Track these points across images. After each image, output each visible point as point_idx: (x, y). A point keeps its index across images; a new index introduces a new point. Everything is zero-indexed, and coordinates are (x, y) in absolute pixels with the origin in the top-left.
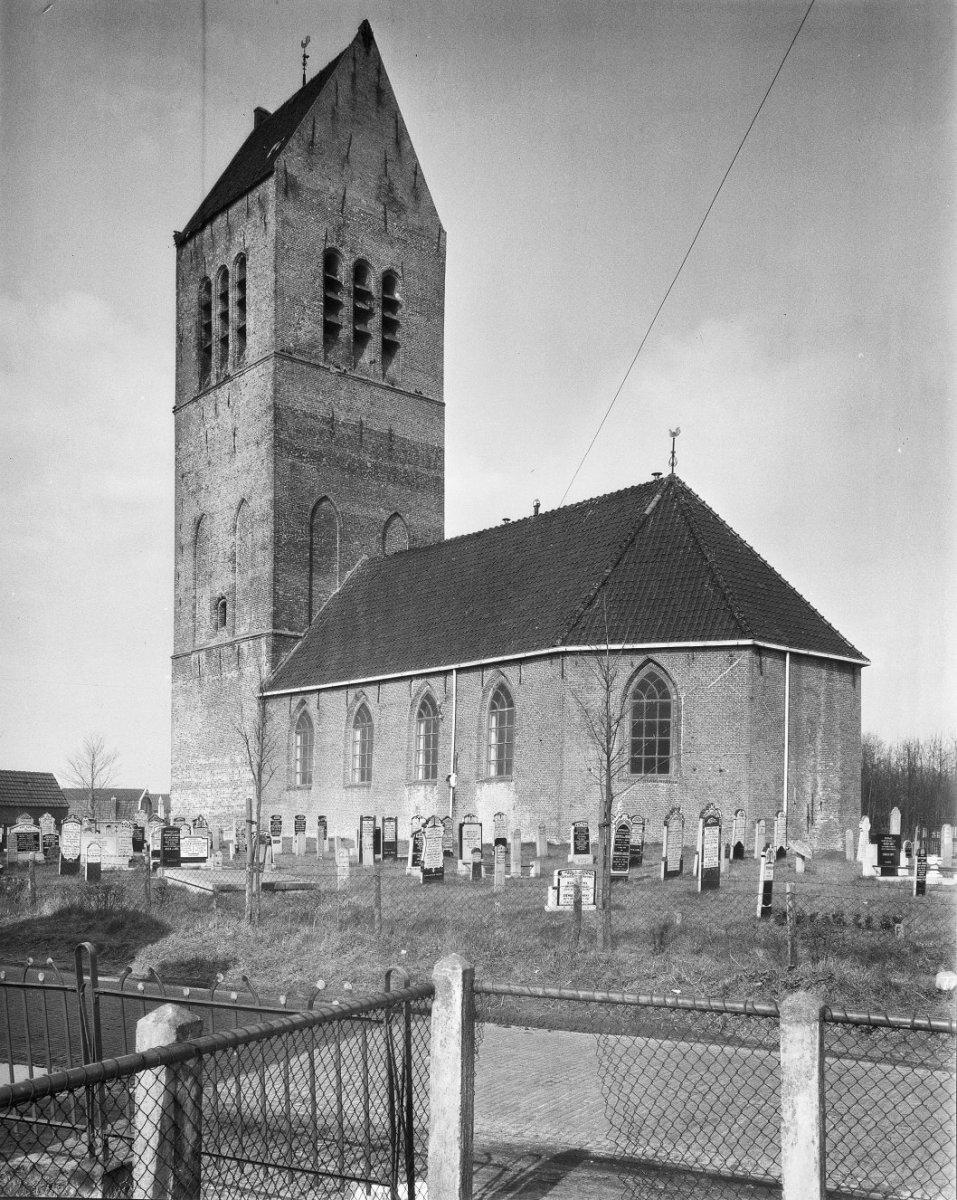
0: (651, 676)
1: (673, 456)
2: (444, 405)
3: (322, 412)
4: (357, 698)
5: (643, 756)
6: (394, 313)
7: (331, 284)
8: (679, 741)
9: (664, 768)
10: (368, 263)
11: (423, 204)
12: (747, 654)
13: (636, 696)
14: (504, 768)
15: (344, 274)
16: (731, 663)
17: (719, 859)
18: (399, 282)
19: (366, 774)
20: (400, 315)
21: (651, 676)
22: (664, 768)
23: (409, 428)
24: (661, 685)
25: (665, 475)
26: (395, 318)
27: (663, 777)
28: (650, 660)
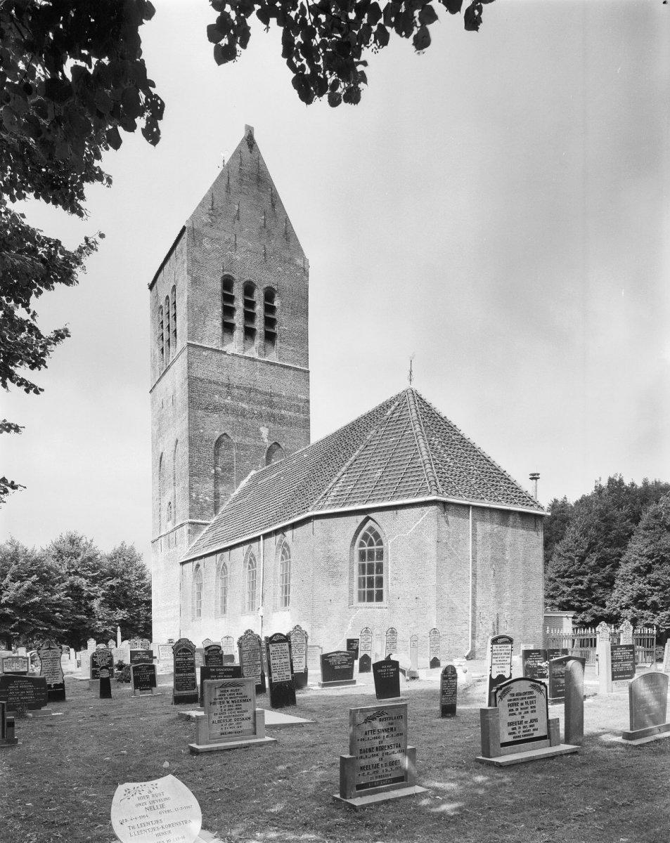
0: (371, 529)
1: (411, 374)
2: (308, 372)
3: (223, 379)
4: (221, 559)
5: (366, 589)
6: (232, 303)
7: (228, 298)
8: (387, 577)
9: (380, 597)
10: (233, 278)
11: (291, 244)
12: (433, 509)
13: (361, 545)
14: (286, 601)
15: (237, 292)
16: (423, 515)
17: (269, 662)
18: (276, 295)
19: (224, 610)
20: (278, 315)
21: (371, 529)
22: (380, 597)
23: (284, 386)
24: (377, 536)
25: (33, 298)
26: (273, 317)
27: (379, 604)
28: (368, 519)
